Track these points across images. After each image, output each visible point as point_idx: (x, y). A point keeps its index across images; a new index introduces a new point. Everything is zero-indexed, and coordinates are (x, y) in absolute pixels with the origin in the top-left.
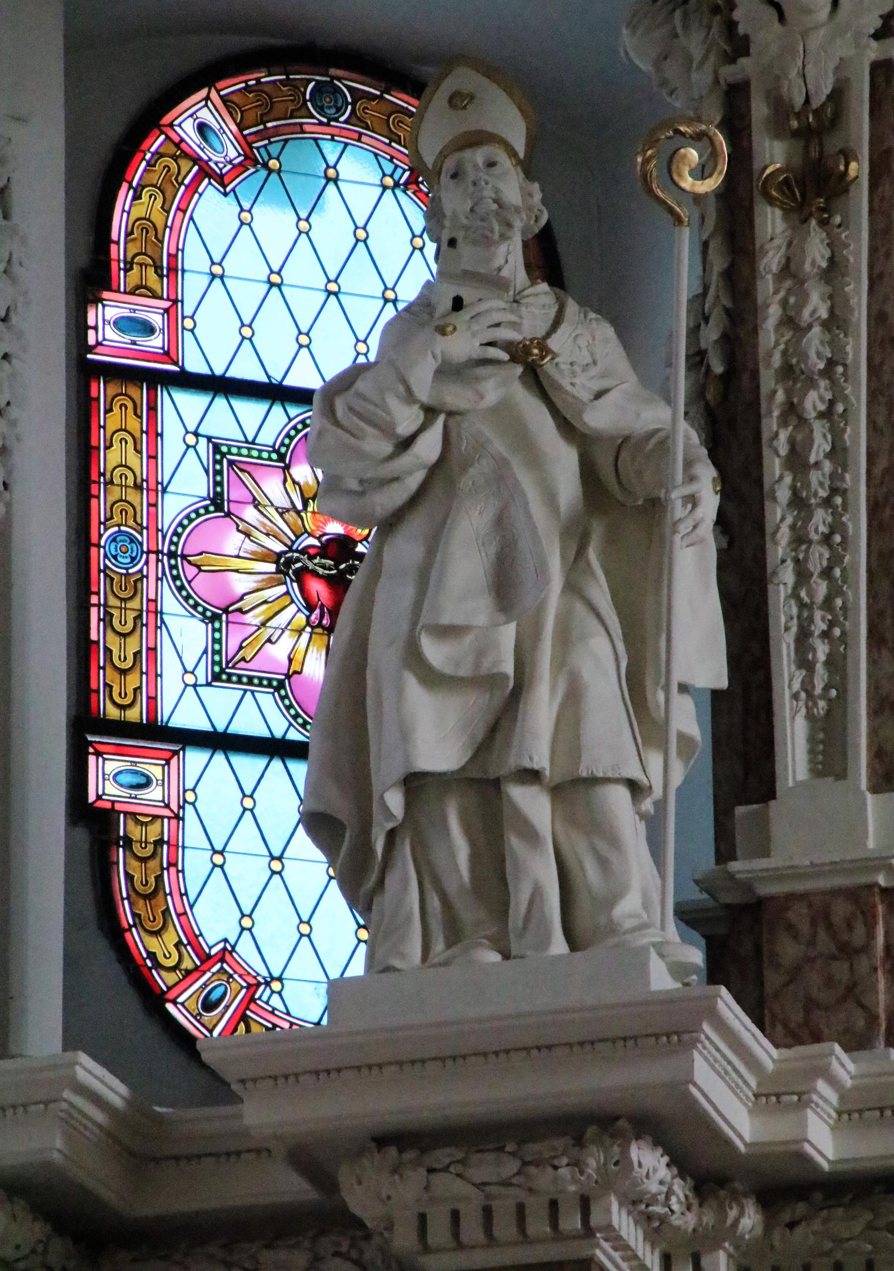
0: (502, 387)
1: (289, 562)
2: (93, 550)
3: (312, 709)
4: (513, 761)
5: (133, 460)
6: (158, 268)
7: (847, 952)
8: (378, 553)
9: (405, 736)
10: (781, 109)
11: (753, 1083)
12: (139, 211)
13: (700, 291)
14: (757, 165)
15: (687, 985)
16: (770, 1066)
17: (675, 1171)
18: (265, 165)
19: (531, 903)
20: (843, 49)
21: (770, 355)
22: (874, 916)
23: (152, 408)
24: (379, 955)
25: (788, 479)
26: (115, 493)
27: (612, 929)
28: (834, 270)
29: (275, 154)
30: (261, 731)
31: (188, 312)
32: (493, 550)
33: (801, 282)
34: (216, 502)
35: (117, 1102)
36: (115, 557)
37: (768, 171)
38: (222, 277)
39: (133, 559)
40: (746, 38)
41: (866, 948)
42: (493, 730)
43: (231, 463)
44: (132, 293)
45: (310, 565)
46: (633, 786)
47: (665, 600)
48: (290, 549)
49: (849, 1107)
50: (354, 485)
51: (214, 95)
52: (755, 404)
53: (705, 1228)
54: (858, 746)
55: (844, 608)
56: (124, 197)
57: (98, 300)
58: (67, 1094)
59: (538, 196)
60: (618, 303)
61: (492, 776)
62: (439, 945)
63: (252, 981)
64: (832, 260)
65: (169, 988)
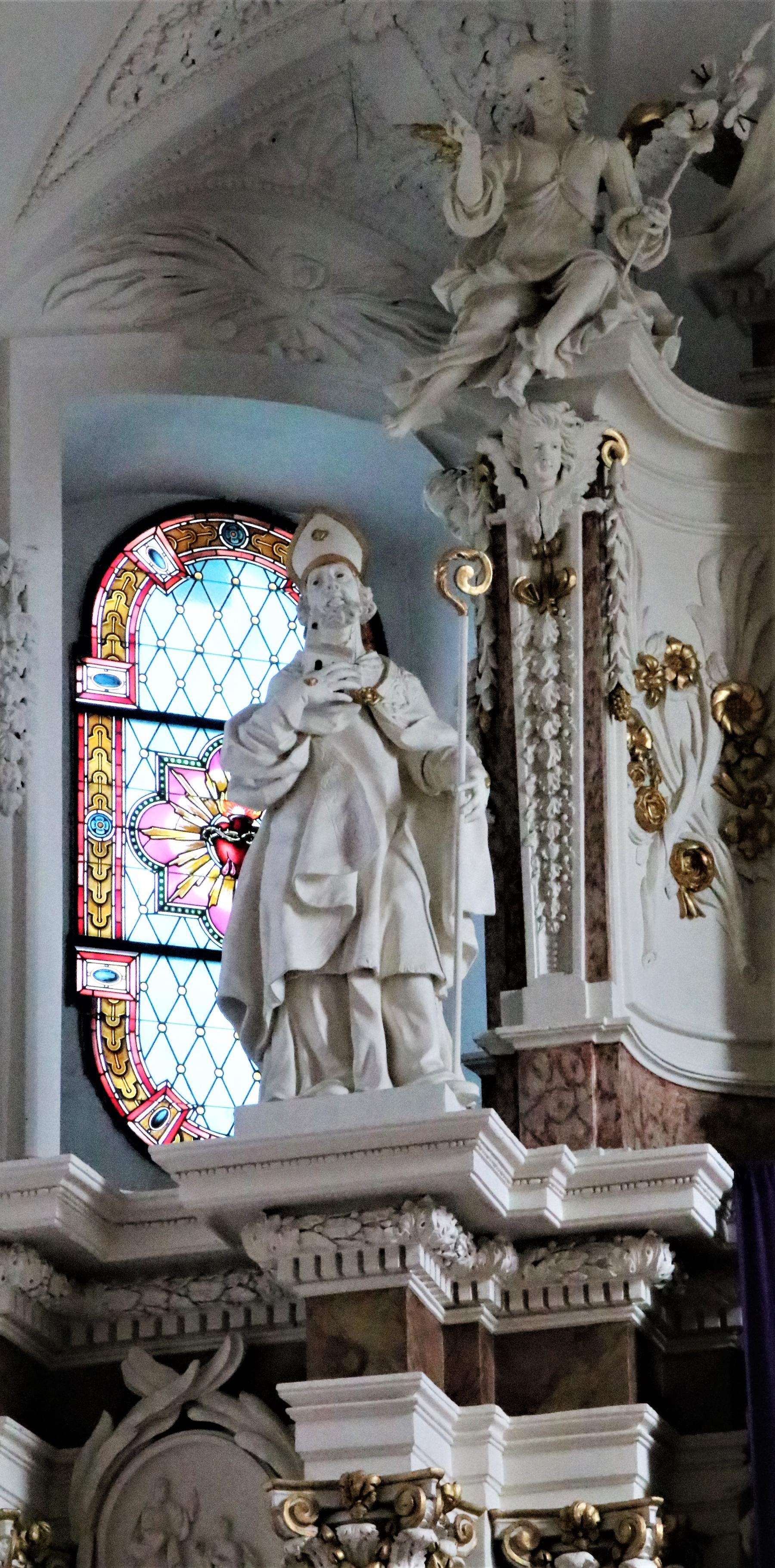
0: (349, 718)
1: (209, 833)
2: (80, 826)
3: (224, 928)
4: (357, 962)
5: (106, 767)
6: (122, 643)
7: (572, 1085)
8: (267, 827)
9: (285, 947)
10: (525, 540)
11: (512, 1171)
12: (110, 605)
13: (475, 657)
14: (511, 577)
15: (469, 1108)
16: (522, 1160)
17: (461, 1229)
18: (193, 576)
19: (368, 1054)
20: (565, 504)
21: (521, 698)
22: (590, 1061)
23: (119, 733)
24: (268, 1088)
25: (534, 779)
26: (94, 789)
27: (421, 1072)
28: (561, 645)
29: (199, 569)
30: (190, 944)
31: (142, 671)
32: (342, 824)
33: (540, 651)
34: (161, 794)
35: (97, 1187)
36: (95, 830)
37: (518, 581)
38: (164, 648)
39: (106, 831)
40: (503, 496)
41: (585, 1084)
42: (343, 942)
43: (171, 769)
44: (106, 659)
45: (223, 835)
46: (434, 978)
47: (455, 852)
48: (210, 825)
49: (573, 1185)
50: (251, 782)
51: (159, 531)
52: (511, 731)
53: (481, 1265)
54: (579, 951)
55: (570, 862)
56: (100, 597)
57: (84, 663)
58: (63, 1182)
59: (370, 596)
60: (422, 667)
61: (341, 973)
62: (307, 1082)
63: (185, 1108)
64: (560, 638)
65: (130, 1112)
